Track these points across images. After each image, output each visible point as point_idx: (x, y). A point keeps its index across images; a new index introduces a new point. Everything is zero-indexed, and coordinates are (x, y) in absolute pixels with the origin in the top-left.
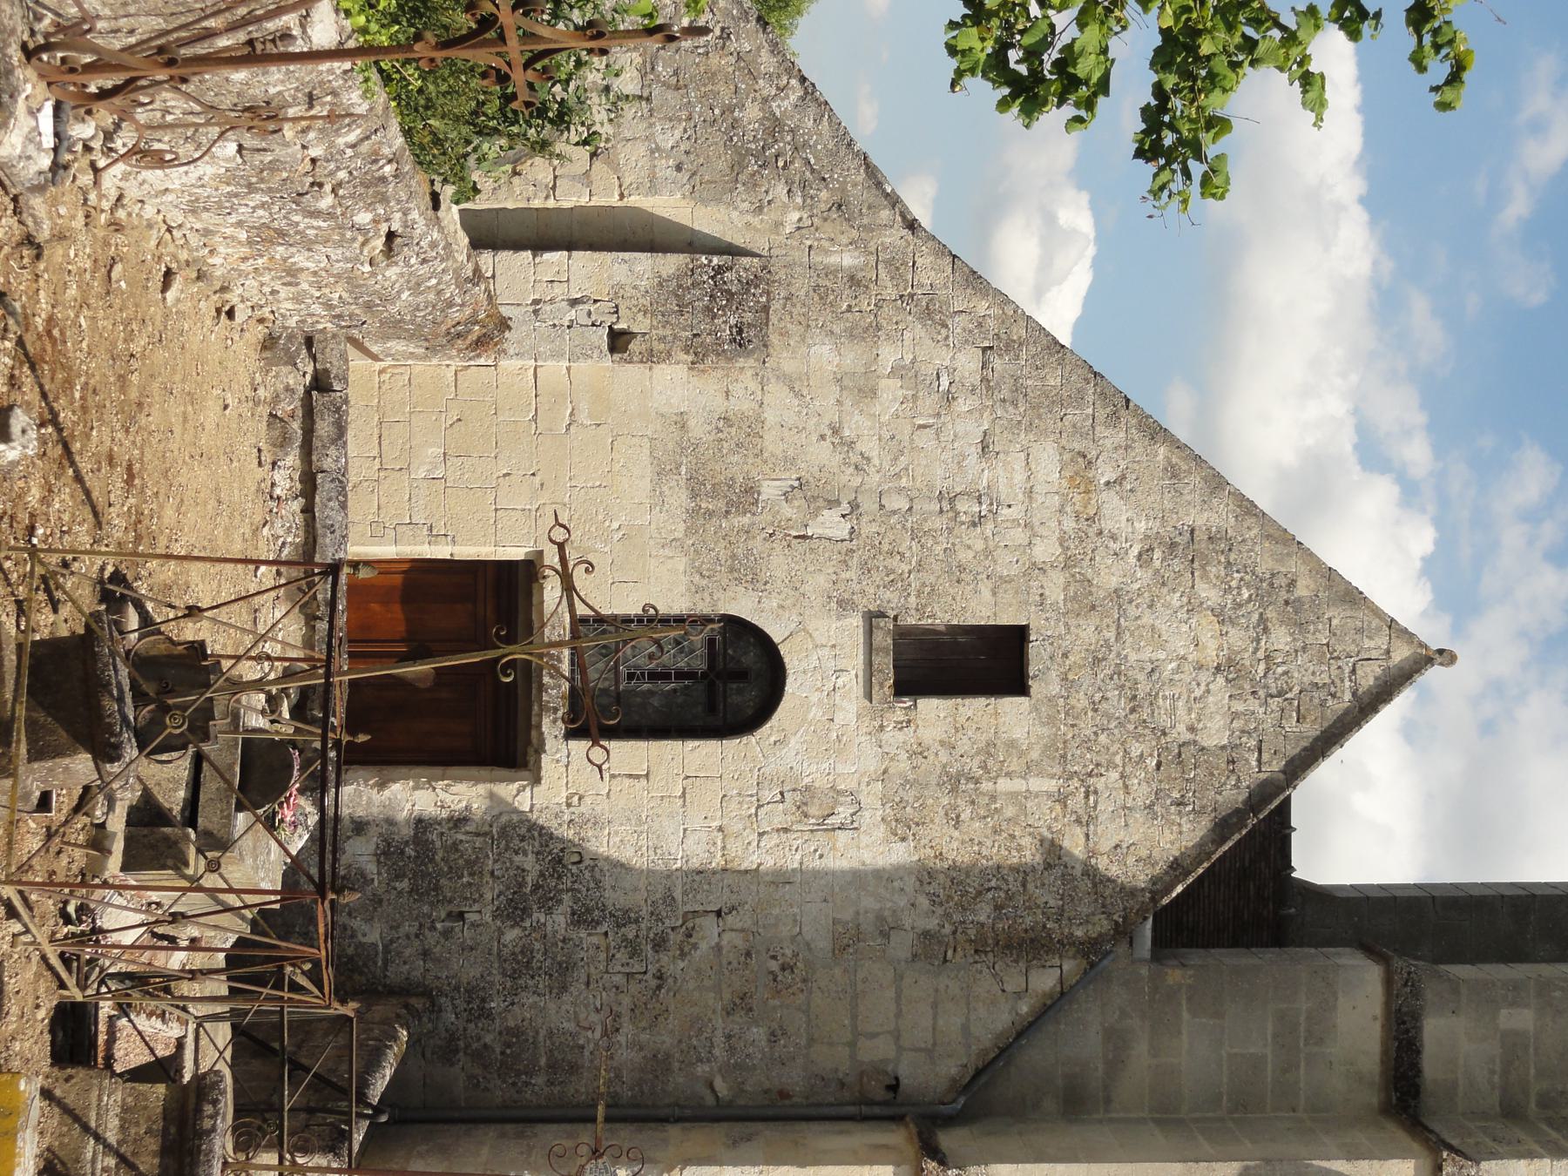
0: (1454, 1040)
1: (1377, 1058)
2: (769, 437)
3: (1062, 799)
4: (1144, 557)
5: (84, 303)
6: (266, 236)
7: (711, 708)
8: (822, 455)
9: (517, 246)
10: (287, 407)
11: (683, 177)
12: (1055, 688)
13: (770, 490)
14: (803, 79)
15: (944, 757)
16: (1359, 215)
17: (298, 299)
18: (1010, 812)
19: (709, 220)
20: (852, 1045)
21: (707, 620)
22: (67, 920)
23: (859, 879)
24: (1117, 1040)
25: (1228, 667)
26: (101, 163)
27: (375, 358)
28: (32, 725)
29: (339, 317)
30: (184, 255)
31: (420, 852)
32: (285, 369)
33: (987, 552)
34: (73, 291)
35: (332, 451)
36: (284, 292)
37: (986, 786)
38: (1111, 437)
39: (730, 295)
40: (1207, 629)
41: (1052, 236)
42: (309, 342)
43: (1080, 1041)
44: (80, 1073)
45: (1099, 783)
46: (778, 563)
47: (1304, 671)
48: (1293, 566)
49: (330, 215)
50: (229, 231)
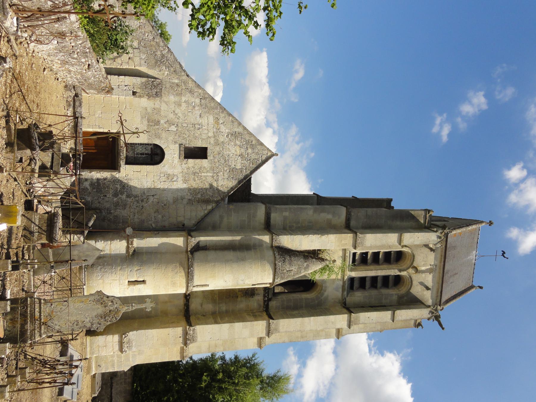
0: (276, 217)
1: (263, 218)
2: (162, 113)
3: (213, 177)
4: (227, 136)
5: (26, 70)
6: (64, 63)
7: (152, 160)
8: (172, 116)
9: (115, 75)
10: (70, 99)
11: (146, 64)
12: (212, 158)
13: (162, 122)
14: (168, 48)
15: (193, 169)
16: (267, 84)
17: (71, 77)
18: (204, 179)
19: (151, 72)
20: (177, 218)
21: (151, 144)
22: (27, 184)
23: (178, 190)
24: (221, 217)
26: (29, 42)
27: (88, 94)
28: (18, 144)
29: (80, 82)
30: (48, 66)
31: (98, 184)
32: (69, 92)
33: (201, 134)
34: (24, 67)
35: (79, 108)
36: (68, 76)
37: (200, 174)
38: (222, 115)
39: (155, 86)
41: (215, 85)
42: (74, 87)
43: (215, 217)
44: (30, 212)
45: (219, 174)
46: (164, 135)
47: (253, 156)
48: (252, 138)
49: (76, 59)
50: (56, 61)
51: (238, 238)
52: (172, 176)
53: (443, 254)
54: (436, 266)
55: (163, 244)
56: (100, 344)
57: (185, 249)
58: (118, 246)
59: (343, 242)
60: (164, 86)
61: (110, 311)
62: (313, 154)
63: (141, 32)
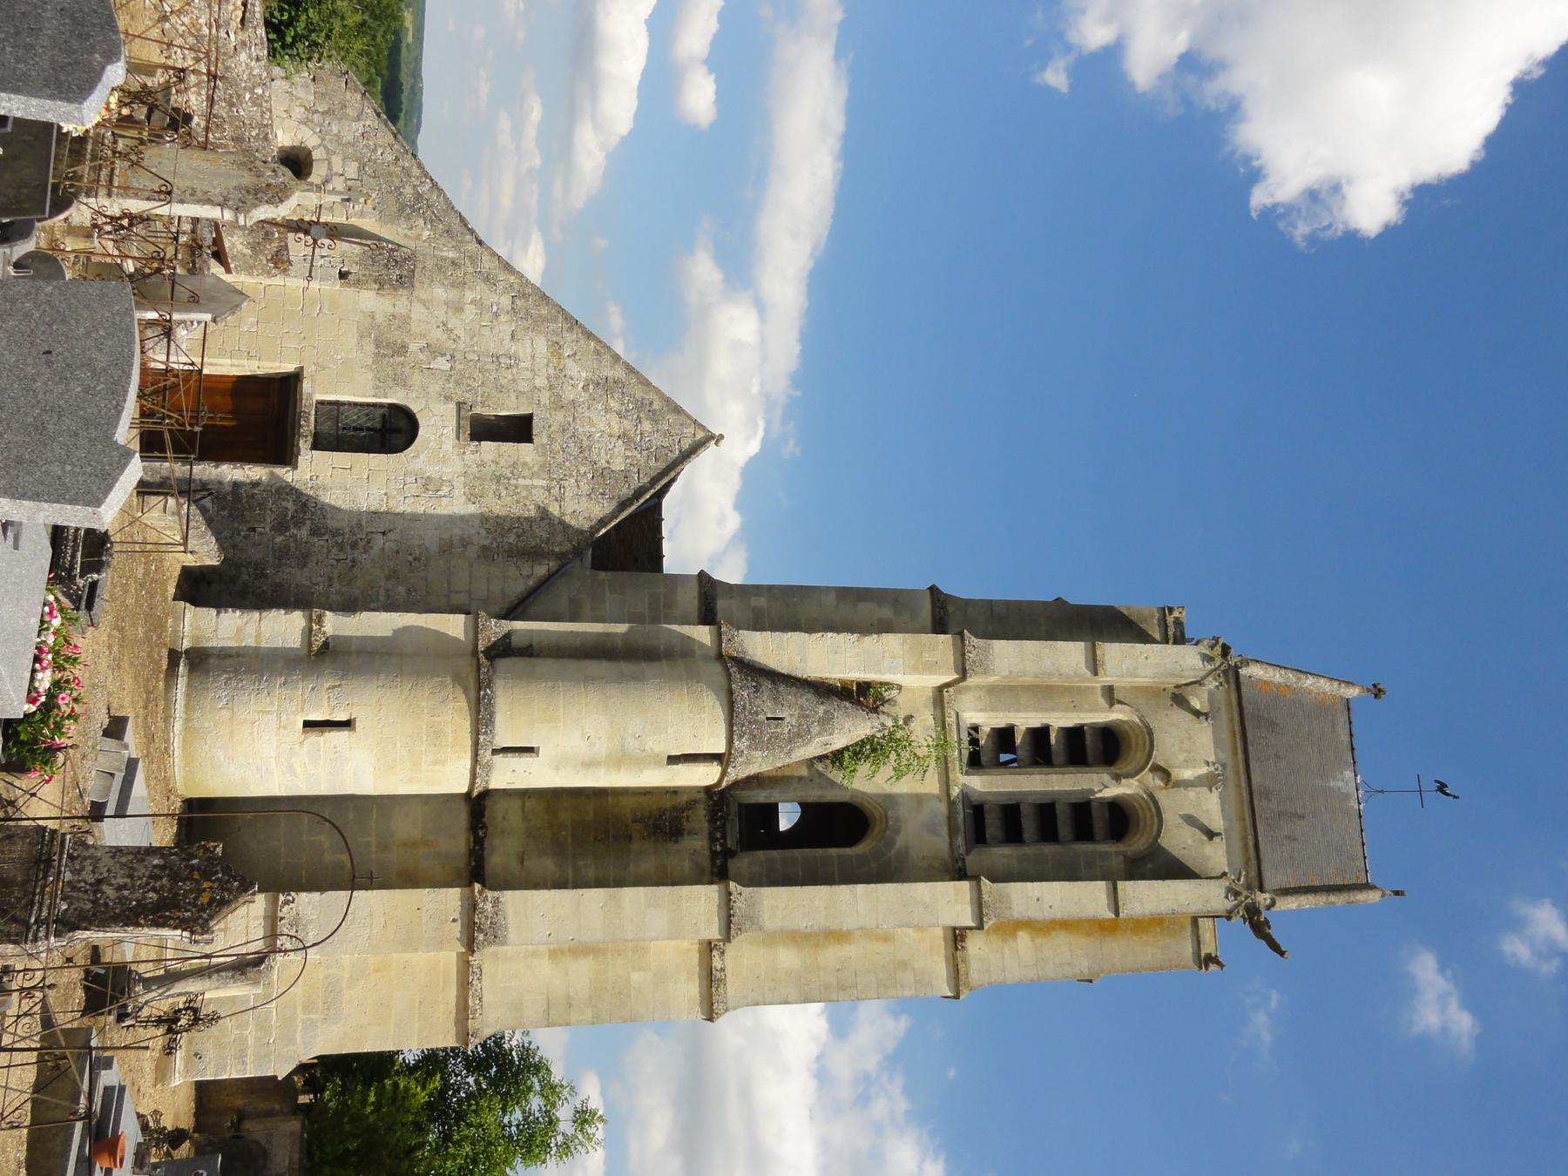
12: (545, 440)
13: (413, 347)
15: (493, 467)
18: (524, 493)
19: (385, 232)
23: (453, 519)
25: (623, 436)
33: (514, 381)
38: (569, 337)
40: (615, 420)
45: (566, 484)
46: (416, 379)
47: (657, 440)
51: (622, 628)
52: (434, 482)
53: (1237, 728)
54: (1224, 766)
55: (405, 629)
57: (470, 648)
58: (282, 628)
59: (926, 657)
60: (420, 266)
61: (268, 185)
62: (952, 1073)
63: (367, 146)
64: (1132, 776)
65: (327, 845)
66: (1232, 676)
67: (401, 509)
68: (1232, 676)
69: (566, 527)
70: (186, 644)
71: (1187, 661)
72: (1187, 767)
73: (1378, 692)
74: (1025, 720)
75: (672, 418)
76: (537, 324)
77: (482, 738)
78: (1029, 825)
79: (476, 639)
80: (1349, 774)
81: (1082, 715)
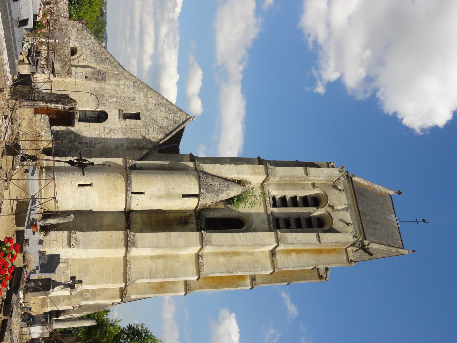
4: (155, 105)
8: (113, 92)
13: (106, 96)
23: (118, 139)
25: (166, 118)
40: (163, 114)
46: (107, 104)
47: (176, 118)
51: (167, 163)
52: (114, 129)
54: (350, 205)
56: (52, 238)
59: (257, 171)
64: (323, 208)
65: (84, 226)
66: (349, 179)
67: (104, 137)
68: (349, 179)
69: (151, 141)
70: (45, 165)
71: (335, 173)
72: (339, 206)
73: (400, 193)
74: (289, 194)
75: (180, 113)
76: (141, 89)
77: (128, 188)
78: (293, 223)
79: (126, 164)
80: (393, 216)
81: (306, 191)
